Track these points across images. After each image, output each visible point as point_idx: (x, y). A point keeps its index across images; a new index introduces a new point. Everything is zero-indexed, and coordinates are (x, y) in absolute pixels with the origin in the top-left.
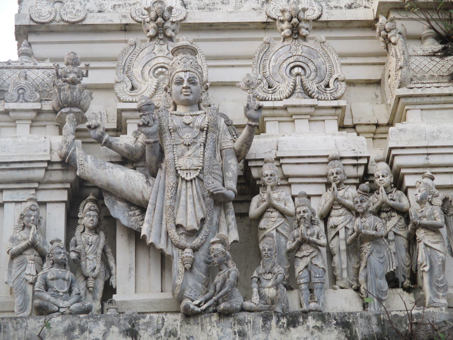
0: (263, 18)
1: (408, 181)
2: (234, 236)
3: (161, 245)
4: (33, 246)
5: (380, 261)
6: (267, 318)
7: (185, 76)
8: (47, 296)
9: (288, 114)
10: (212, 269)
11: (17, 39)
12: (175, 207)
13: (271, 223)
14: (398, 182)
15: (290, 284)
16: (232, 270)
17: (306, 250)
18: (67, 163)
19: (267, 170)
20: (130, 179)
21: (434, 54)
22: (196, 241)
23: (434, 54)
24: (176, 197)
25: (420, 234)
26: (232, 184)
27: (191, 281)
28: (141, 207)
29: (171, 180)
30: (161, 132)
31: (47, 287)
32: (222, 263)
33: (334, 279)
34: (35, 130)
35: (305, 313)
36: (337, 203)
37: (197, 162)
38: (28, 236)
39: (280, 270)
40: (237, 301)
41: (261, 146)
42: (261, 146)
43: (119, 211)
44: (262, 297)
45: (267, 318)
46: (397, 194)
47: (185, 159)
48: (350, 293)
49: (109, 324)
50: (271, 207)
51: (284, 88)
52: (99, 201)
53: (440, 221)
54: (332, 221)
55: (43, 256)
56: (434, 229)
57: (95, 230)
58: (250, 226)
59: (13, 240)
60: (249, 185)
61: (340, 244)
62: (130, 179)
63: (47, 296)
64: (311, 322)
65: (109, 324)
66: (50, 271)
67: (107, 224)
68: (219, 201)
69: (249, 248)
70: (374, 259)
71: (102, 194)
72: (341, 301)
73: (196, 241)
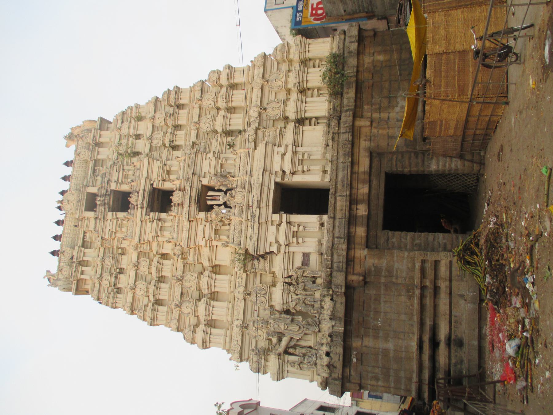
0: (243, 301)
1: (290, 275)
2: (300, 317)
3: (302, 335)
4: (299, 365)
5: (310, 285)
6: (321, 313)
7: (261, 325)
8: (312, 363)
9: (270, 299)
10: (309, 324)
11: (54, 256)
12: (293, 331)
13: (298, 308)
14: (290, 277)
15: (313, 306)
16: (309, 320)
17: (306, 301)
18: (279, 355)
19: (285, 307)
20: (285, 341)
21: (259, 263)
22: (302, 327)
23: (259, 263)
24: (291, 330)
25: (304, 275)
26: (288, 316)
27: (311, 329)
28: (292, 338)
29: (287, 331)
30: (274, 332)
31: (309, 362)
32: (308, 322)
33: (312, 295)
34: (269, 360)
35: (321, 305)
36: (294, 293)
37: (283, 325)
38: (296, 365)
39: (310, 308)
40: (316, 319)
41: (278, 307)
42: (278, 307)
43: (292, 344)
44: (315, 313)
45: (321, 313)
46: (293, 278)
47: (282, 327)
48: (316, 292)
49: (320, 349)
50: (294, 308)
51: (263, 299)
52: (289, 348)
53: (302, 271)
54: (298, 293)
55: (301, 363)
56: (304, 272)
57: (295, 349)
58: (299, 313)
59: (297, 369)
60: (287, 312)
61: (304, 293)
62: (285, 341)
63: (312, 363)
64: (323, 303)
65: (320, 349)
66: (306, 361)
67: (295, 347)
68: (293, 320)
69: (304, 315)
70: (309, 286)
71: (287, 347)
72: (317, 295)
73: (302, 327)
